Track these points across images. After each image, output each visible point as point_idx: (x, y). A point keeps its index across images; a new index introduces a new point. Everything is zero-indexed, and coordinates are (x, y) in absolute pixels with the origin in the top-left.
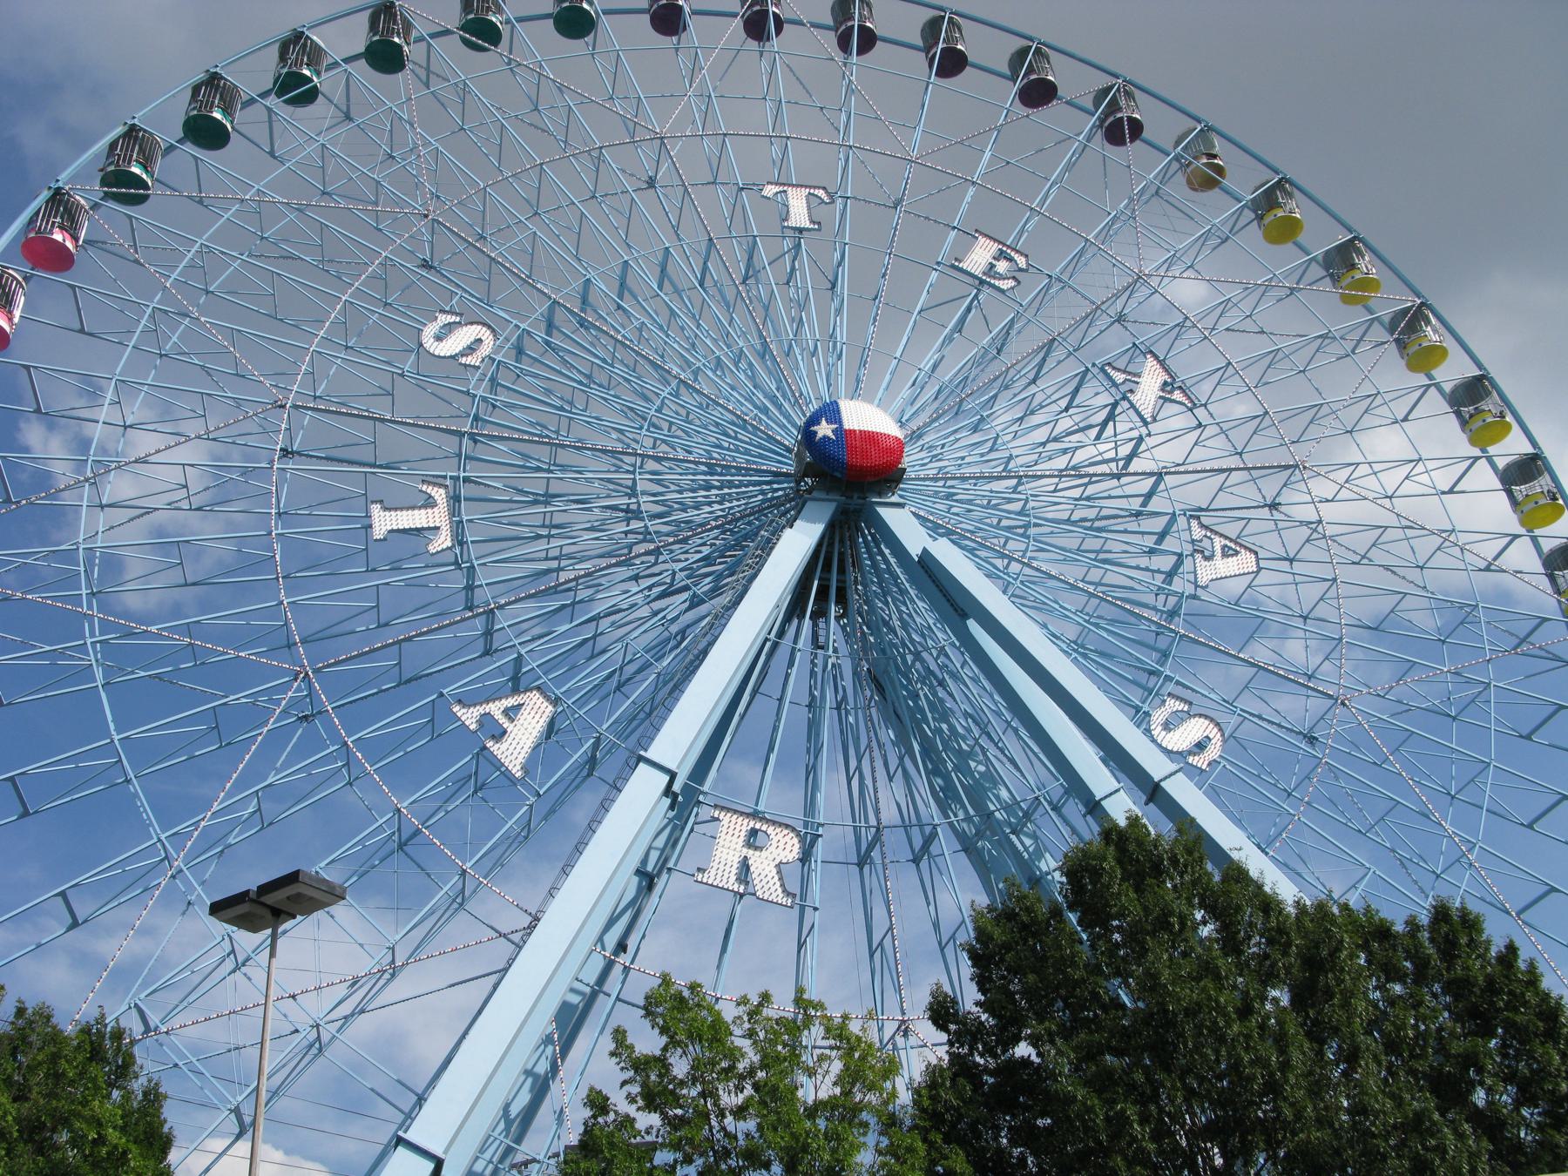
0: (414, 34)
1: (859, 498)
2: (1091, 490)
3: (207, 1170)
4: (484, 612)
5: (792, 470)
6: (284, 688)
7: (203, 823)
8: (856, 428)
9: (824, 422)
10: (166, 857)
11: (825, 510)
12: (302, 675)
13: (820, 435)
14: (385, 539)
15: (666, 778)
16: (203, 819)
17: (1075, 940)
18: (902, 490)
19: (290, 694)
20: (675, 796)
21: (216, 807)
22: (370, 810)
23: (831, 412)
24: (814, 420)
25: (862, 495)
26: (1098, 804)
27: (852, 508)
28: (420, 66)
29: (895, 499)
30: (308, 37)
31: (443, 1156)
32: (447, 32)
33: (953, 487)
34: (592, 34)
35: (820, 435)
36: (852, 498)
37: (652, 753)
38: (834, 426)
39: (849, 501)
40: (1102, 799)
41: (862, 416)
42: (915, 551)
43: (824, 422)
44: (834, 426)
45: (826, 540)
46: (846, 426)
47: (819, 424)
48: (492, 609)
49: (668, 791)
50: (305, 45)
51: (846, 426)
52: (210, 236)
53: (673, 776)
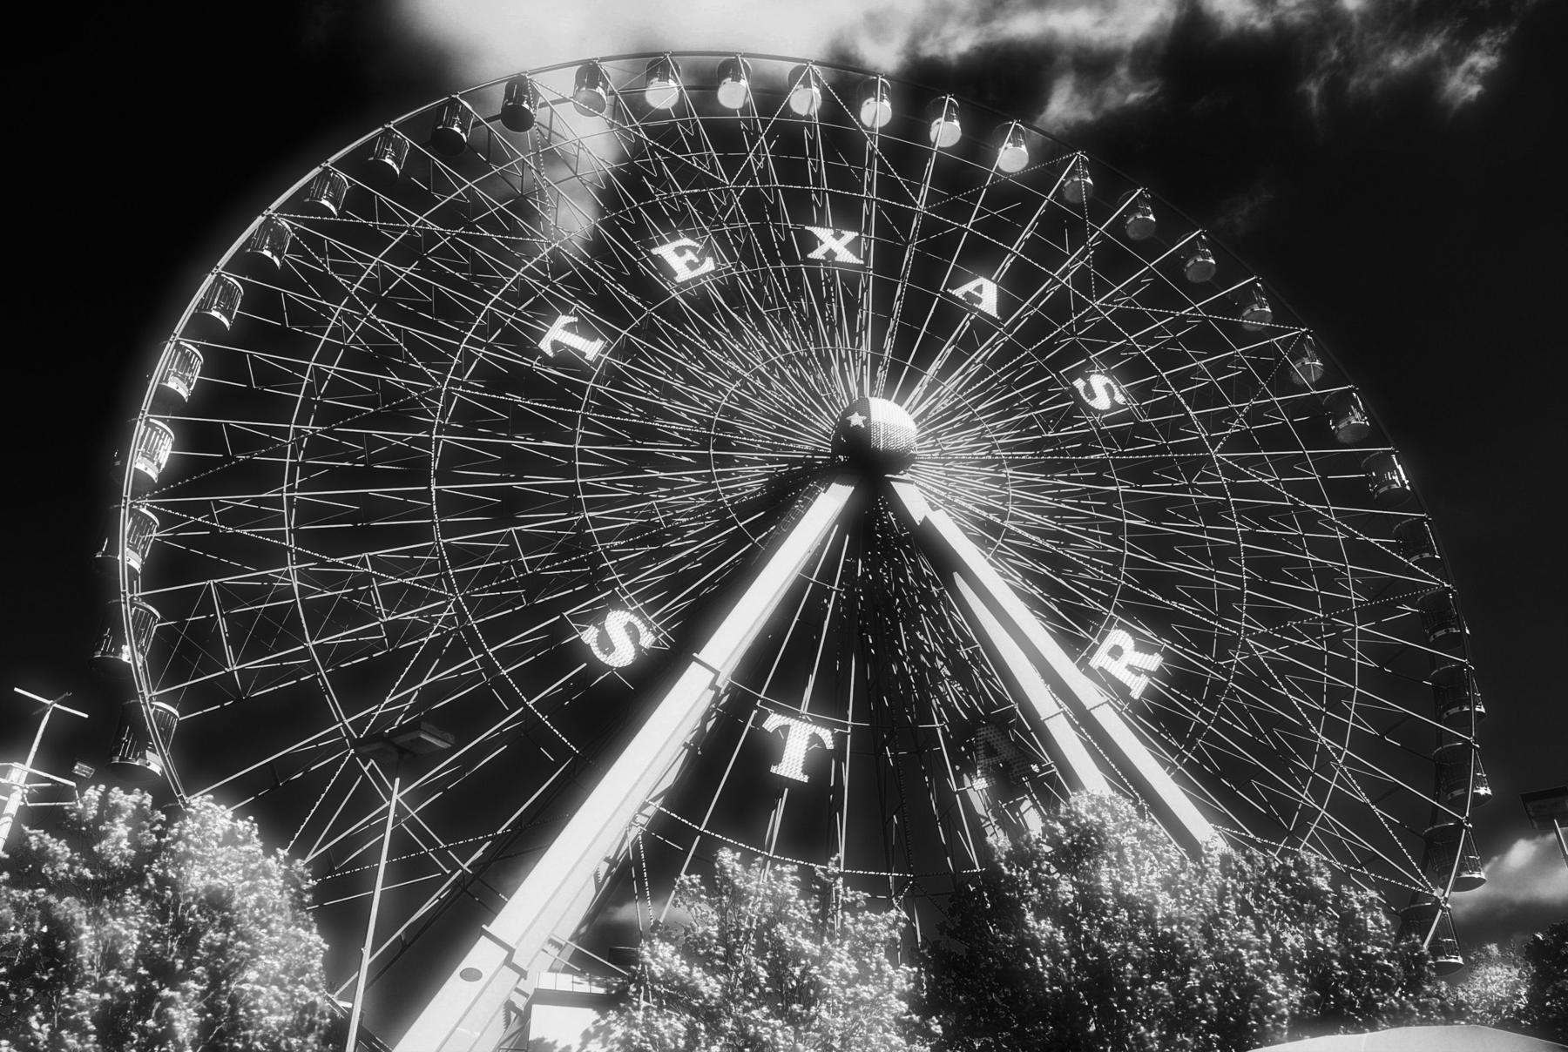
0: (541, 100)
2: (1167, 528)
3: (471, 1049)
6: (442, 609)
15: (712, 675)
17: (1350, 996)
18: (913, 468)
20: (718, 689)
21: (388, 700)
24: (849, 412)
28: (544, 127)
29: (904, 477)
31: (514, 947)
32: (564, 100)
33: (951, 467)
37: (703, 655)
38: (865, 418)
44: (865, 418)
49: (713, 686)
53: (717, 673)
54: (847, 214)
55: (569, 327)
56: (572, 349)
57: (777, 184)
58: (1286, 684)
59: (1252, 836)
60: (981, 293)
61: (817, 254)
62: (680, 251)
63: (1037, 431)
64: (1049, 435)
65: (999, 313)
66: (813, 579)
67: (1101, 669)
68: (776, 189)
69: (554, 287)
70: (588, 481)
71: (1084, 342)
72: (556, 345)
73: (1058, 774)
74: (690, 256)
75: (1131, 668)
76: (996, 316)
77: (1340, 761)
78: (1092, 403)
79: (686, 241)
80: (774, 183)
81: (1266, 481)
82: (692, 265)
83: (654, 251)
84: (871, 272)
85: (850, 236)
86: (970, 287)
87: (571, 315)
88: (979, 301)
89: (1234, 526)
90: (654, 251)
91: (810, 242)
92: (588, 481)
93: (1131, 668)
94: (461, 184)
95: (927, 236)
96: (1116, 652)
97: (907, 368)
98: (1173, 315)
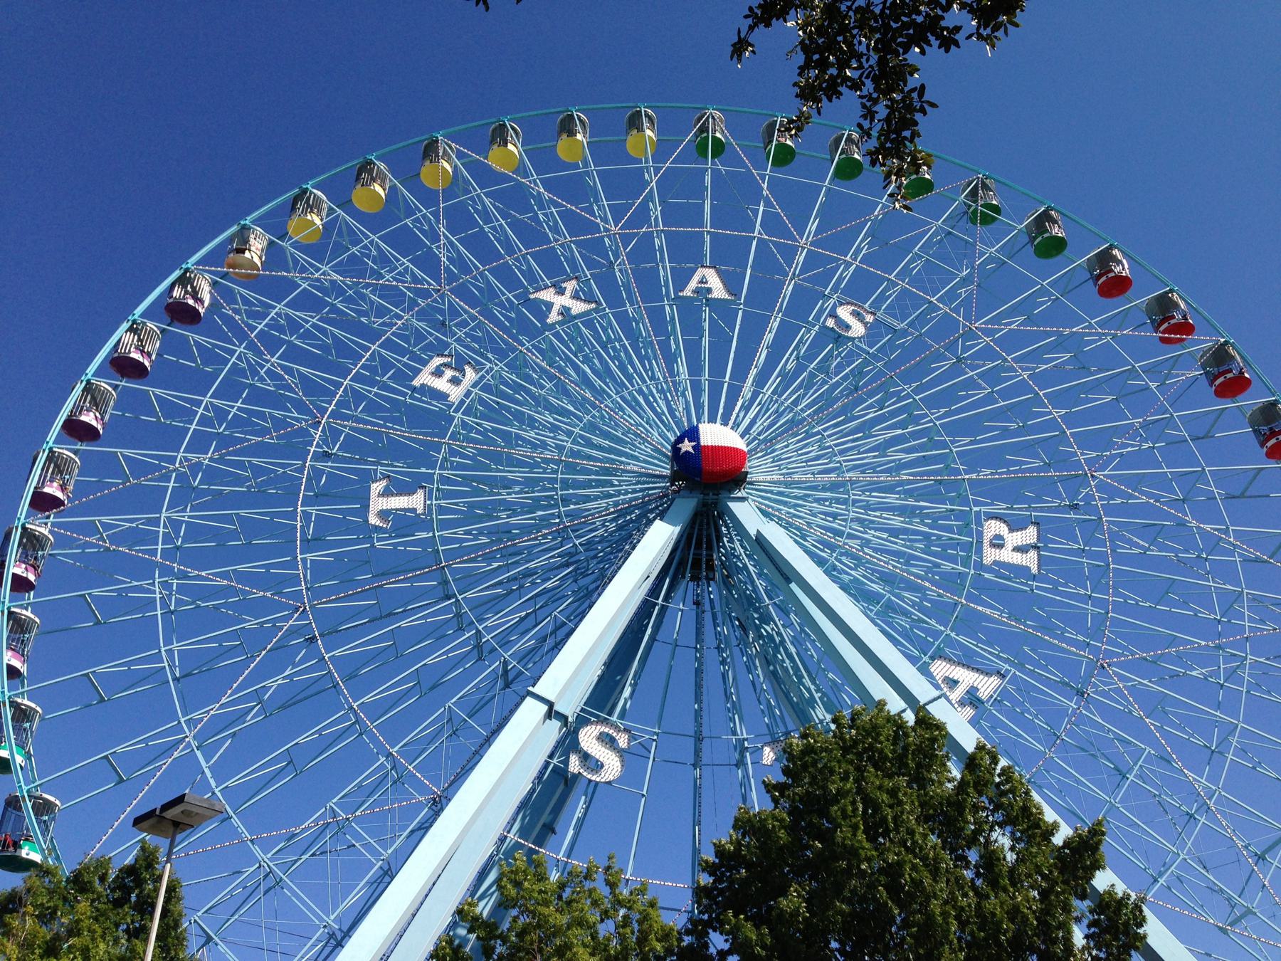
1: (713, 494)
4: (438, 569)
5: (667, 472)
7: (212, 712)
8: (710, 444)
9: (686, 440)
10: (357, 721)
11: (686, 506)
12: (301, 609)
13: (684, 450)
14: (771, 765)
16: (212, 709)
19: (291, 622)
21: (224, 700)
22: (1155, 663)
23: (693, 434)
25: (716, 492)
26: (923, 707)
27: (710, 501)
30: (311, 193)
34: (711, 945)
35: (684, 450)
36: (708, 494)
39: (707, 497)
40: (926, 704)
41: (714, 434)
42: (753, 532)
43: (686, 440)
45: (682, 543)
46: (702, 444)
47: (683, 442)
48: (443, 567)
50: (309, 199)
51: (702, 444)
52: (280, 355)
54: (556, 273)
55: (386, 493)
56: (401, 510)
57: (524, 251)
58: (1142, 493)
59: (1203, 643)
60: (706, 283)
61: (553, 317)
62: (438, 373)
63: (824, 382)
64: (834, 381)
65: (731, 294)
66: (560, 476)
67: (995, 562)
68: (524, 257)
69: (358, 420)
70: (443, 503)
71: (804, 280)
72: (383, 514)
73: (1017, 673)
74: (449, 373)
75: (1017, 549)
76: (727, 297)
77: (1232, 540)
78: (850, 334)
79: (438, 361)
80: (520, 250)
81: (1014, 326)
82: (455, 381)
83: (416, 383)
84: (607, 311)
85: (570, 286)
86: (693, 284)
87: (380, 480)
88: (709, 290)
89: (1021, 375)
90: (416, 383)
91: (543, 309)
92: (443, 503)
93: (1017, 549)
94: (232, 407)
95: (124, 410)
96: (998, 543)
97: (726, 385)
98: (869, 220)
